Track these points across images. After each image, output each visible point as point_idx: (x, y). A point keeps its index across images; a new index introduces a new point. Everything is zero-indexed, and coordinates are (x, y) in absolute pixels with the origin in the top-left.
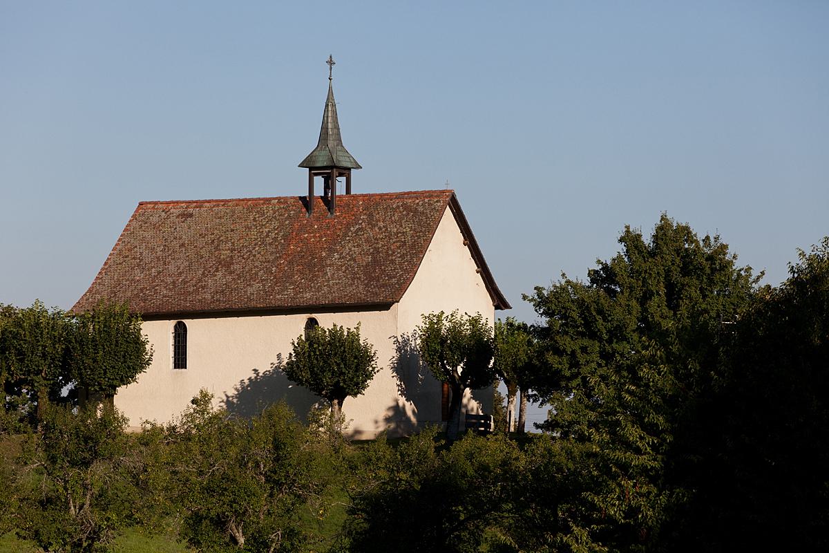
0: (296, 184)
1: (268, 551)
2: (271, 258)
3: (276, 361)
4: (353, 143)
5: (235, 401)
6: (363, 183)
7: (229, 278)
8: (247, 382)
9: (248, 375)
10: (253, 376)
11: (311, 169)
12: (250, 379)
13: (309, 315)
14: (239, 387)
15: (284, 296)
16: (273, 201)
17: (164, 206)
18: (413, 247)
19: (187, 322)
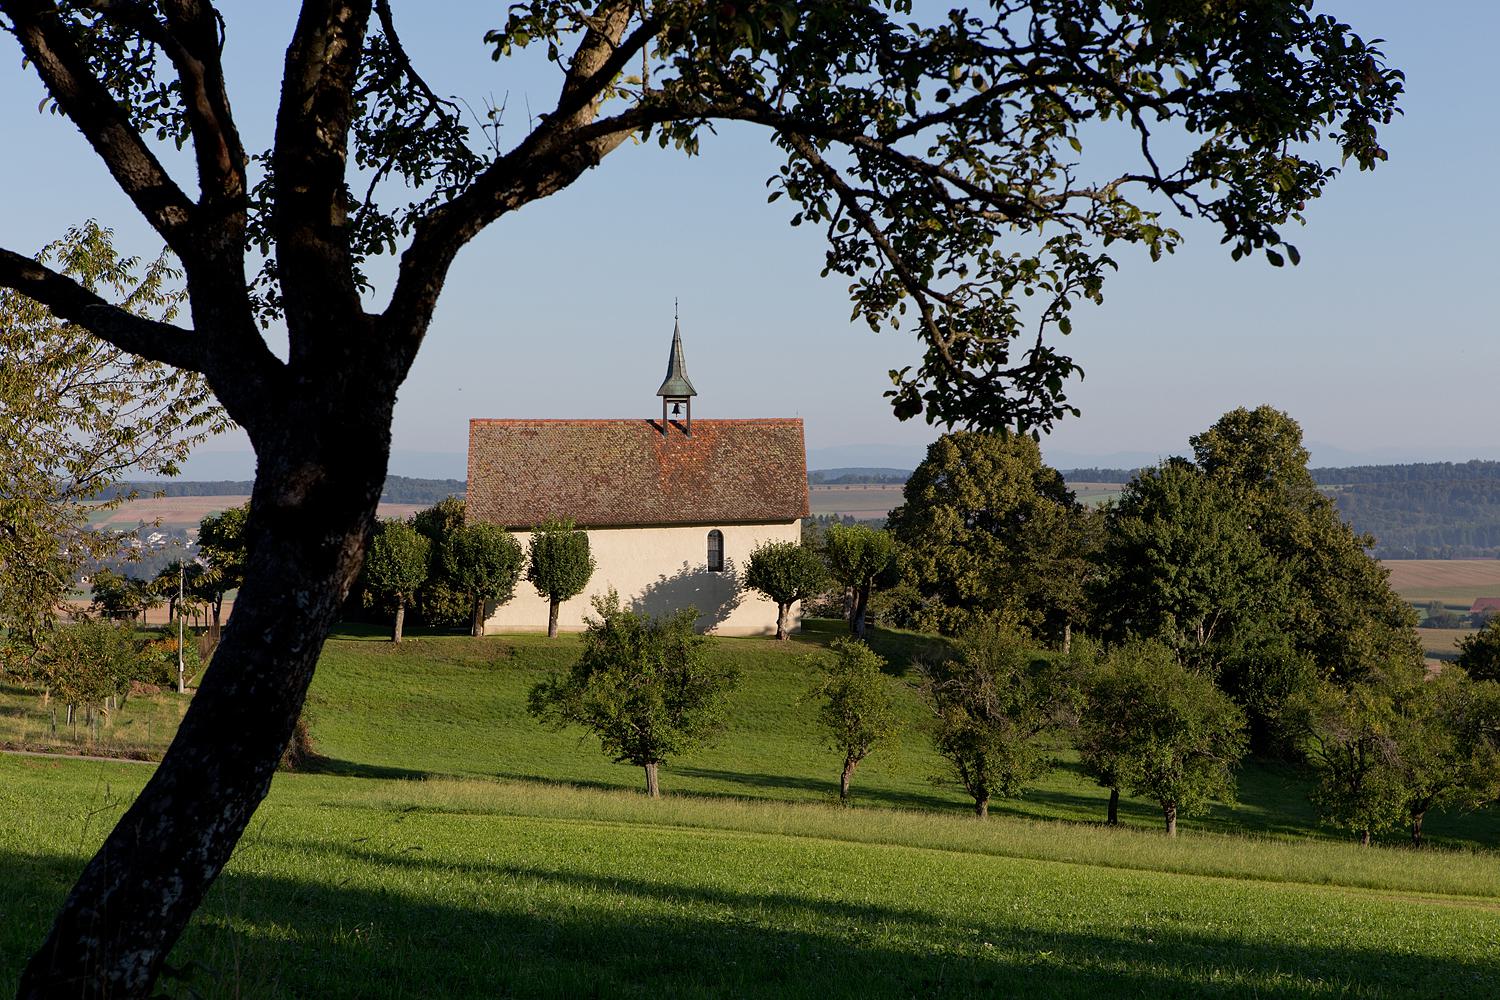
0: (654, 409)
1: (1493, 707)
2: (650, 475)
3: (683, 568)
4: (693, 369)
5: (642, 603)
6: (701, 409)
7: (616, 493)
8: (653, 586)
9: (653, 579)
10: (660, 580)
11: (665, 397)
12: (656, 584)
13: (711, 528)
14: (645, 590)
15: (688, 511)
16: (517, 423)
17: (501, 424)
18: (792, 467)
19: (723, 529)
